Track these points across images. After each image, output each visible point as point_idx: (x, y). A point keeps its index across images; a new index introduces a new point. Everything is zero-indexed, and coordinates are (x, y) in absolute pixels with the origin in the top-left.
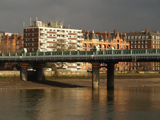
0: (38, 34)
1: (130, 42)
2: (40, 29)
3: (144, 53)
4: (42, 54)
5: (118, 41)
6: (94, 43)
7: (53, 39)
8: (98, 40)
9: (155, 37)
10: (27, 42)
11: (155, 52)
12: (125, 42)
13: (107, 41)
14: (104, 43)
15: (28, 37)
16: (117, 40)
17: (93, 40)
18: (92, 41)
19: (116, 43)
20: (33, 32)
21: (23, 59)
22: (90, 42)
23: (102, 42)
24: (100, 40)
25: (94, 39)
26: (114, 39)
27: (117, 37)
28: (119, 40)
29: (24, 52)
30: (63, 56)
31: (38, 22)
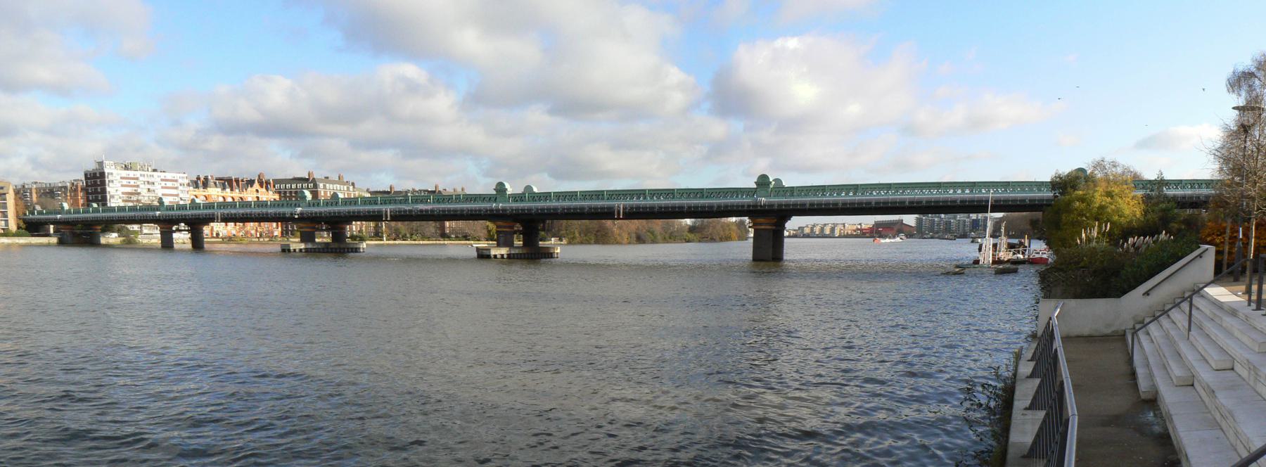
0: (105, 181)
1: (280, 193)
2: (108, 174)
4: (112, 209)
5: (257, 191)
7: (134, 188)
8: (219, 190)
9: (325, 186)
10: (91, 194)
12: (271, 193)
13: (237, 191)
14: (232, 195)
15: (91, 186)
16: (255, 190)
20: (98, 178)
22: (204, 194)
23: (226, 193)
24: (224, 189)
25: (211, 189)
26: (249, 189)
27: (255, 185)
28: (259, 190)
31: (107, 162)
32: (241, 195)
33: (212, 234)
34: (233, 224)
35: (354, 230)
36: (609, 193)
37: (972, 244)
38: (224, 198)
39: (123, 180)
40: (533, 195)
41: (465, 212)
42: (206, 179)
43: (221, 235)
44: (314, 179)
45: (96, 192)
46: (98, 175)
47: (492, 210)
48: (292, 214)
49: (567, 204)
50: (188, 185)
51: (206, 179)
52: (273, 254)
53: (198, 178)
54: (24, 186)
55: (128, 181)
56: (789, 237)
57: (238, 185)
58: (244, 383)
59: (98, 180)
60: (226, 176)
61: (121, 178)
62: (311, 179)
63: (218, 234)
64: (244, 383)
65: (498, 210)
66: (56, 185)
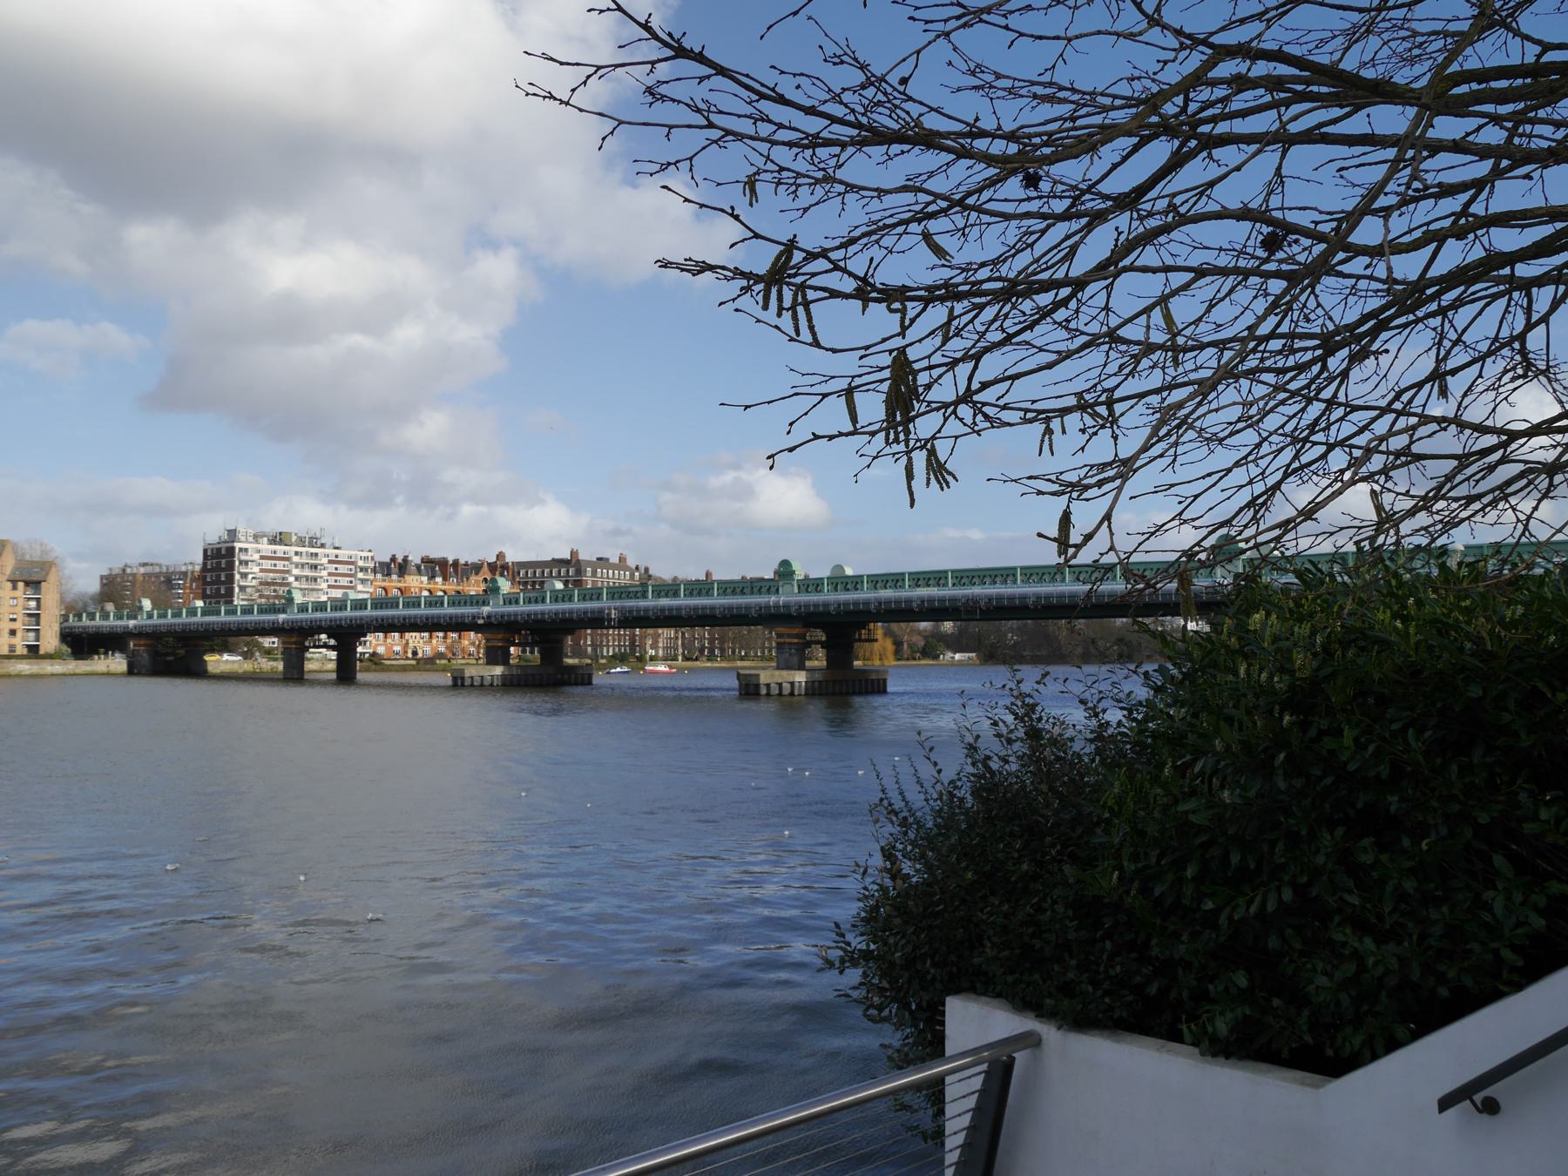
0: (233, 562)
2: (241, 550)
3: (598, 599)
6: (410, 587)
8: (425, 579)
11: (599, 597)
16: (481, 579)
17: (407, 577)
18: (405, 582)
19: (479, 586)
20: (223, 557)
21: (323, 623)
24: (431, 578)
25: (412, 577)
27: (481, 573)
29: (141, 608)
30: (401, 612)
32: (460, 588)
33: (406, 652)
34: (441, 634)
35: (589, 638)
36: (955, 575)
37: (748, 705)
38: (430, 591)
39: (263, 561)
40: (845, 580)
41: (683, 612)
42: (405, 559)
43: (420, 655)
44: (578, 561)
45: (217, 581)
46: (223, 552)
47: (768, 607)
48: (474, 617)
49: (887, 594)
50: (374, 571)
51: (405, 559)
52: (447, 688)
53: (393, 559)
54: (124, 570)
55: (273, 562)
56: (633, 637)
57: (456, 571)
58: (434, 880)
59: (224, 561)
60: (435, 554)
61: (262, 558)
62: (574, 561)
63: (415, 653)
64: (434, 880)
65: (777, 606)
66: (177, 570)
